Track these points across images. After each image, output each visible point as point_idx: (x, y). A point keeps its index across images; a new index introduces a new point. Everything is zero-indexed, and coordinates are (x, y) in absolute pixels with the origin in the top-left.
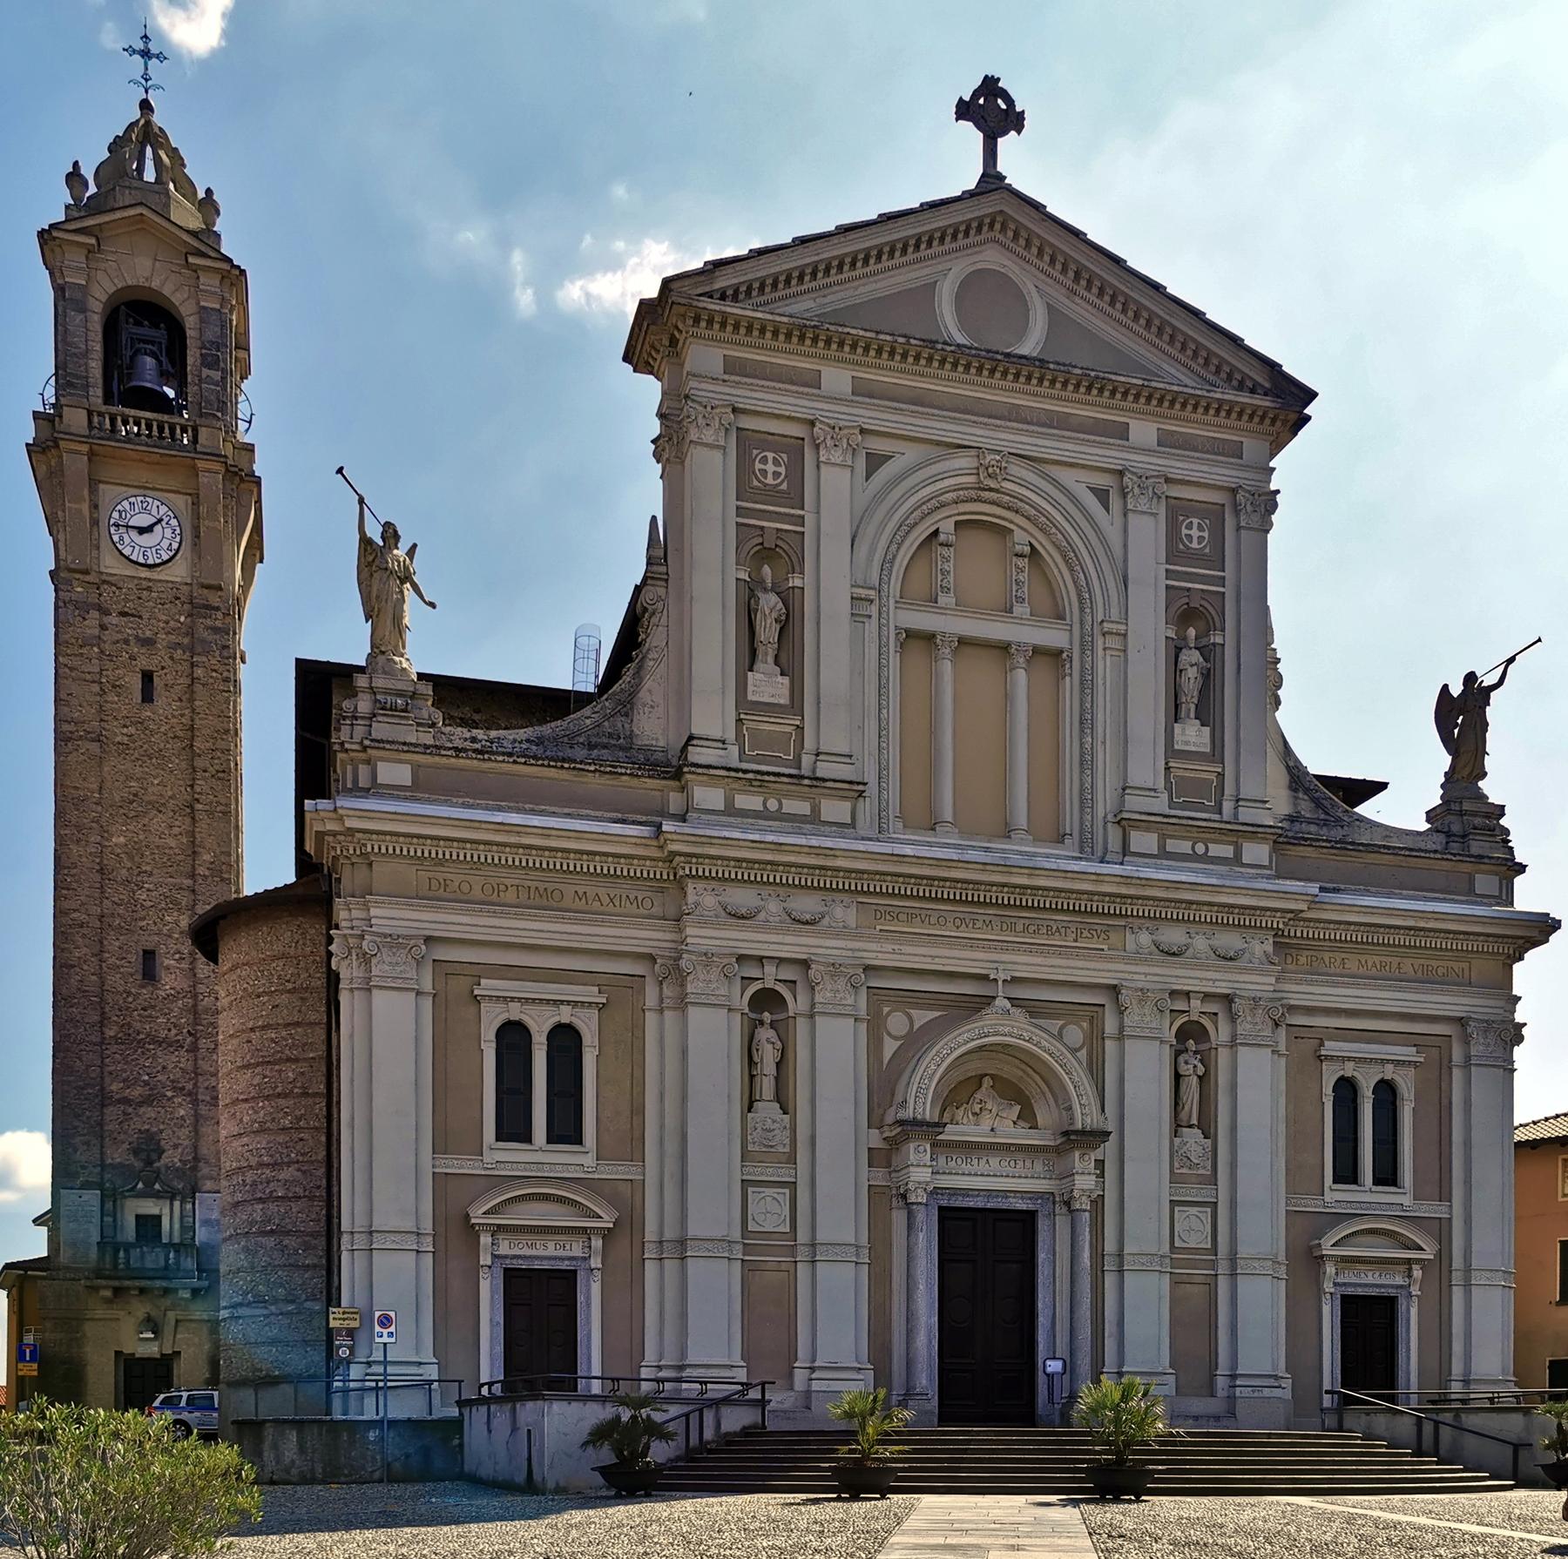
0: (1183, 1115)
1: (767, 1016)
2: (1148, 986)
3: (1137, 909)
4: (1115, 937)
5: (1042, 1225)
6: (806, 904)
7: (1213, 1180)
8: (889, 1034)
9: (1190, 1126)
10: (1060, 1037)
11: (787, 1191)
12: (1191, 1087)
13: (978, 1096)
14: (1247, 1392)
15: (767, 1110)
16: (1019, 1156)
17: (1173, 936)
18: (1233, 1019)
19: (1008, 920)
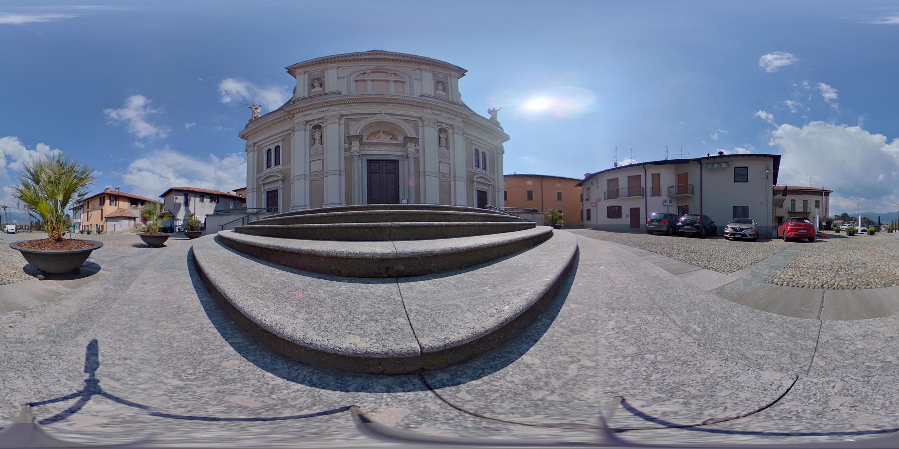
5: (400, 163)
15: (317, 145)
18: (453, 129)
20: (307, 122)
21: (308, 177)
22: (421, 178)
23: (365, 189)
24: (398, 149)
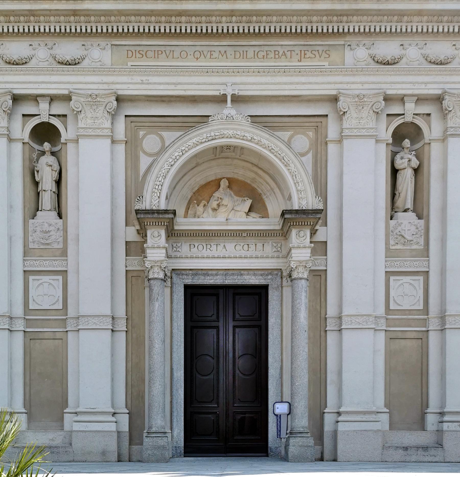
0: (399, 203)
1: (47, 146)
2: (364, 92)
3: (353, 26)
4: (335, 56)
5: (273, 296)
6: (69, 49)
7: (425, 252)
8: (145, 153)
9: (405, 211)
10: (288, 144)
11: (60, 278)
12: (406, 180)
13: (217, 194)
14: (453, 426)
15: (47, 217)
16: (251, 241)
17: (387, 48)
18: (444, 114)
19: (241, 49)
20: (17, 99)
21: (20, 325)
22: (331, 338)
23: (180, 374)
24: (269, 249)
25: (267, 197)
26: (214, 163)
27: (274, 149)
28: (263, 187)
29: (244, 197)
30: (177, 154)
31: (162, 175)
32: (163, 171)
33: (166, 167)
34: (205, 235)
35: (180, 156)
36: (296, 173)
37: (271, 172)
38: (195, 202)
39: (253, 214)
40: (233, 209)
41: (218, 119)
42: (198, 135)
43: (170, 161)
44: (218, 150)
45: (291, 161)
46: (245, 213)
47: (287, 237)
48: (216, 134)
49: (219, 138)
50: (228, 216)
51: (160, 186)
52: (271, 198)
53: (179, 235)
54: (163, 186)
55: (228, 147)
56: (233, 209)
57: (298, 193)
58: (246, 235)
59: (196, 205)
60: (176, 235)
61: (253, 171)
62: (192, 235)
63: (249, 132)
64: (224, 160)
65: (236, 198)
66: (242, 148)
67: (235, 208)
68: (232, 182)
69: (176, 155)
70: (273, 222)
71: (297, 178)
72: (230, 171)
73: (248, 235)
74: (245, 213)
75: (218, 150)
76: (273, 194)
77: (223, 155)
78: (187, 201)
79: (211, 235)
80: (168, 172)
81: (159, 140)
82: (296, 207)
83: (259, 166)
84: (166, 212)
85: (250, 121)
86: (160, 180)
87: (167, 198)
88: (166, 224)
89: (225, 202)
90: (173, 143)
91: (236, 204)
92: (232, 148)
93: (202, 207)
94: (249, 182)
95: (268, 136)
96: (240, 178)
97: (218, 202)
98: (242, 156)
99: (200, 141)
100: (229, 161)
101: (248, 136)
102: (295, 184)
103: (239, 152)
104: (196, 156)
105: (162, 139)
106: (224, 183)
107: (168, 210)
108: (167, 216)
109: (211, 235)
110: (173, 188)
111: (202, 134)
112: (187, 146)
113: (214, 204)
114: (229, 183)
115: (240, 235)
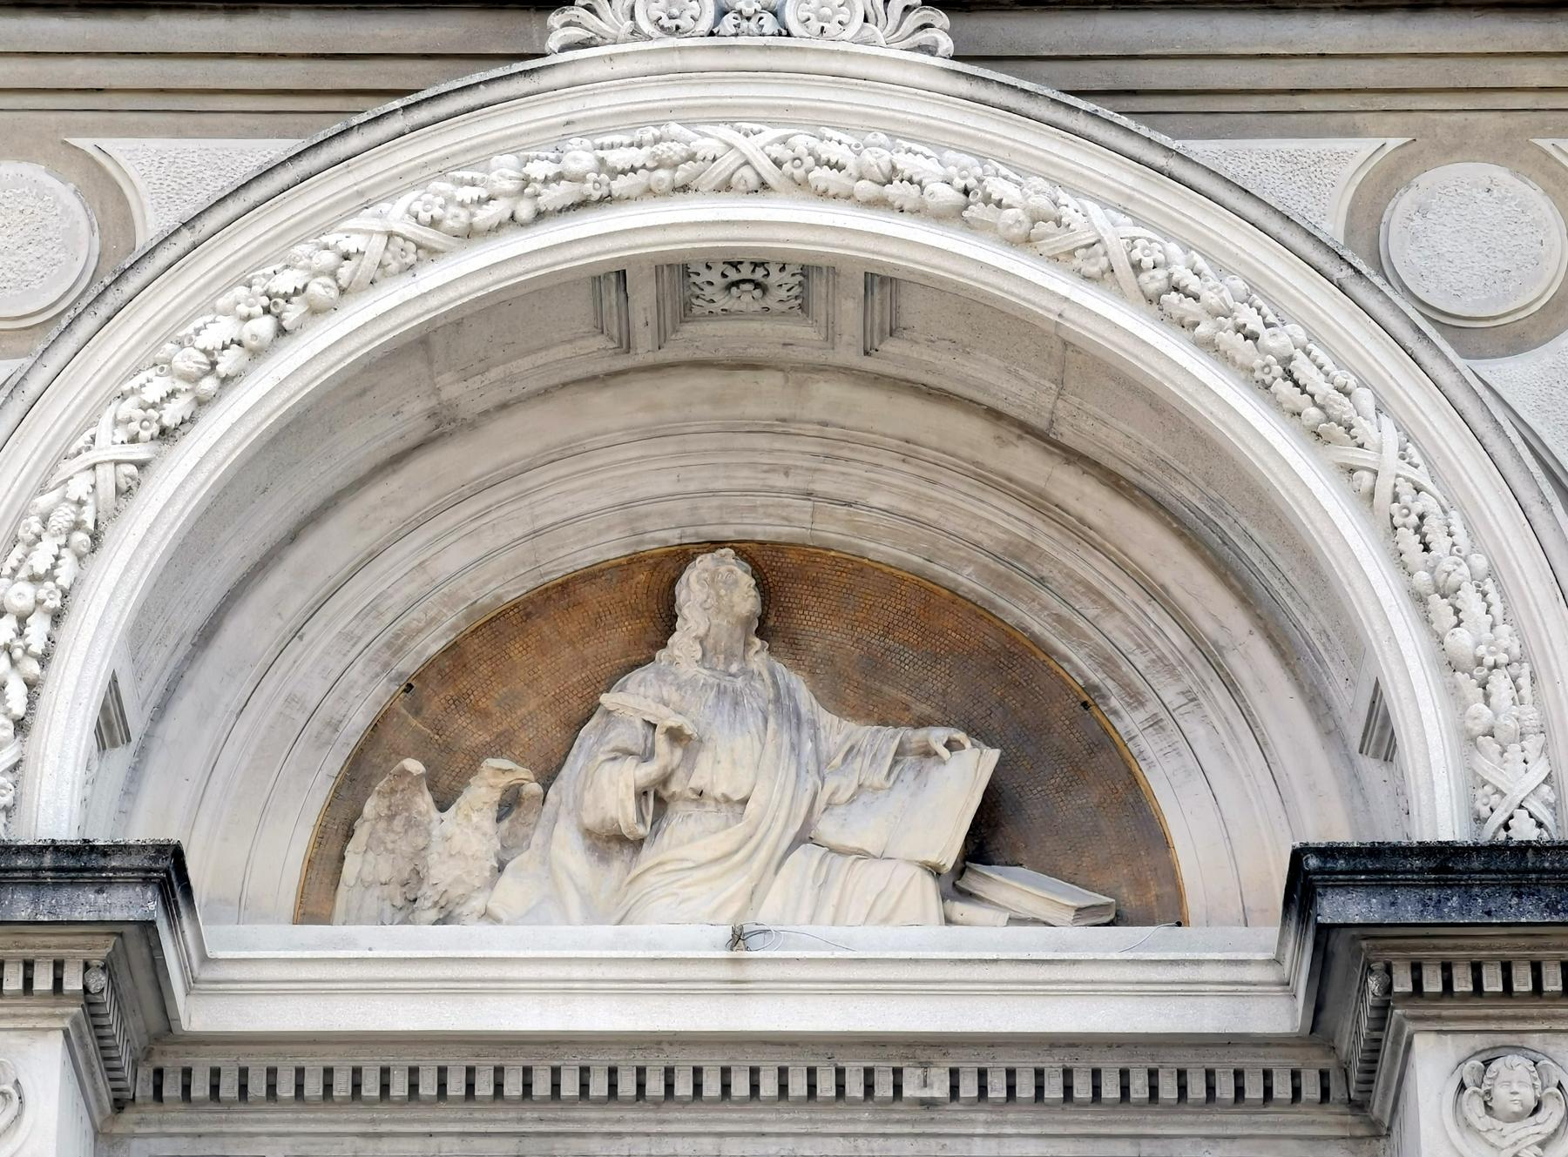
13: (635, 699)
25: (1155, 723)
26: (609, 411)
27: (1193, 284)
28: (1110, 625)
29: (921, 722)
30: (218, 331)
31: (63, 517)
32: (79, 487)
33: (110, 443)
34: (513, 1087)
35: (257, 354)
36: (1425, 503)
37: (1182, 492)
38: (414, 766)
39: (1008, 886)
40: (805, 837)
41: (636, 32)
42: (441, 168)
43: (153, 393)
44: (643, 295)
45: (1365, 398)
46: (935, 871)
47: (1379, 1106)
48: (618, 158)
49: (649, 192)
50: (754, 895)
51: (38, 628)
52: (1196, 730)
53: (229, 1089)
54: (69, 624)
55: (747, 272)
56: (805, 837)
57: (1453, 693)
58: (940, 1090)
59: (425, 801)
60: (200, 1089)
61: (1005, 485)
62: (371, 1088)
63: (935, 140)
64: (707, 382)
65: (837, 731)
66: (881, 284)
67: (827, 828)
68: (786, 589)
69: (211, 339)
70: (1224, 971)
71: (1440, 543)
72: (779, 481)
73: (969, 1088)
74: (935, 871)
75: (643, 295)
76: (1219, 692)
77: (705, 336)
78: (335, 762)
79: (570, 1087)
80: (123, 493)
81: (75, 204)
82: (1442, 821)
83: (1068, 437)
84: (79, 863)
85: (946, 44)
86: (41, 561)
87: (110, 728)
88: (73, 983)
89: (717, 771)
90: (186, 238)
91: (842, 783)
92: (775, 277)
93: (485, 819)
94: (967, 579)
95: (1126, 177)
96: (882, 550)
97: (651, 770)
98: (891, 347)
99: (456, 219)
100: (764, 396)
101: (938, 177)
102: (1420, 599)
103: (850, 311)
104: (421, 347)
105: (105, 194)
106: (714, 596)
107: (105, 851)
108: (86, 904)
109: (570, 1087)
110: (191, 628)
111: (480, 155)
112: (329, 258)
113: (606, 785)
114: (764, 587)
115: (884, 1089)
